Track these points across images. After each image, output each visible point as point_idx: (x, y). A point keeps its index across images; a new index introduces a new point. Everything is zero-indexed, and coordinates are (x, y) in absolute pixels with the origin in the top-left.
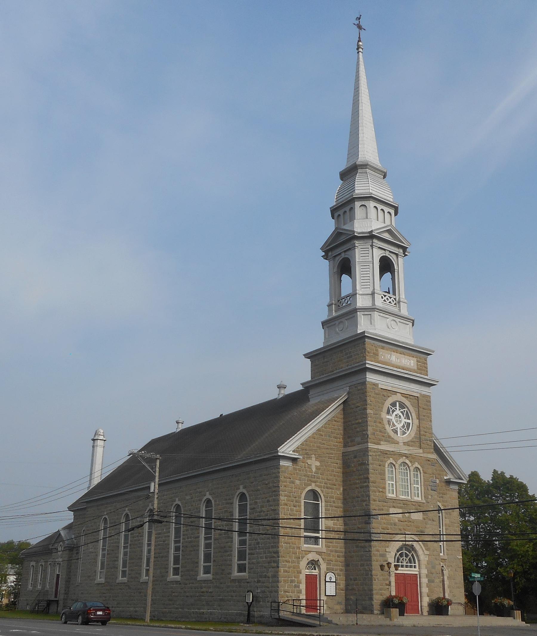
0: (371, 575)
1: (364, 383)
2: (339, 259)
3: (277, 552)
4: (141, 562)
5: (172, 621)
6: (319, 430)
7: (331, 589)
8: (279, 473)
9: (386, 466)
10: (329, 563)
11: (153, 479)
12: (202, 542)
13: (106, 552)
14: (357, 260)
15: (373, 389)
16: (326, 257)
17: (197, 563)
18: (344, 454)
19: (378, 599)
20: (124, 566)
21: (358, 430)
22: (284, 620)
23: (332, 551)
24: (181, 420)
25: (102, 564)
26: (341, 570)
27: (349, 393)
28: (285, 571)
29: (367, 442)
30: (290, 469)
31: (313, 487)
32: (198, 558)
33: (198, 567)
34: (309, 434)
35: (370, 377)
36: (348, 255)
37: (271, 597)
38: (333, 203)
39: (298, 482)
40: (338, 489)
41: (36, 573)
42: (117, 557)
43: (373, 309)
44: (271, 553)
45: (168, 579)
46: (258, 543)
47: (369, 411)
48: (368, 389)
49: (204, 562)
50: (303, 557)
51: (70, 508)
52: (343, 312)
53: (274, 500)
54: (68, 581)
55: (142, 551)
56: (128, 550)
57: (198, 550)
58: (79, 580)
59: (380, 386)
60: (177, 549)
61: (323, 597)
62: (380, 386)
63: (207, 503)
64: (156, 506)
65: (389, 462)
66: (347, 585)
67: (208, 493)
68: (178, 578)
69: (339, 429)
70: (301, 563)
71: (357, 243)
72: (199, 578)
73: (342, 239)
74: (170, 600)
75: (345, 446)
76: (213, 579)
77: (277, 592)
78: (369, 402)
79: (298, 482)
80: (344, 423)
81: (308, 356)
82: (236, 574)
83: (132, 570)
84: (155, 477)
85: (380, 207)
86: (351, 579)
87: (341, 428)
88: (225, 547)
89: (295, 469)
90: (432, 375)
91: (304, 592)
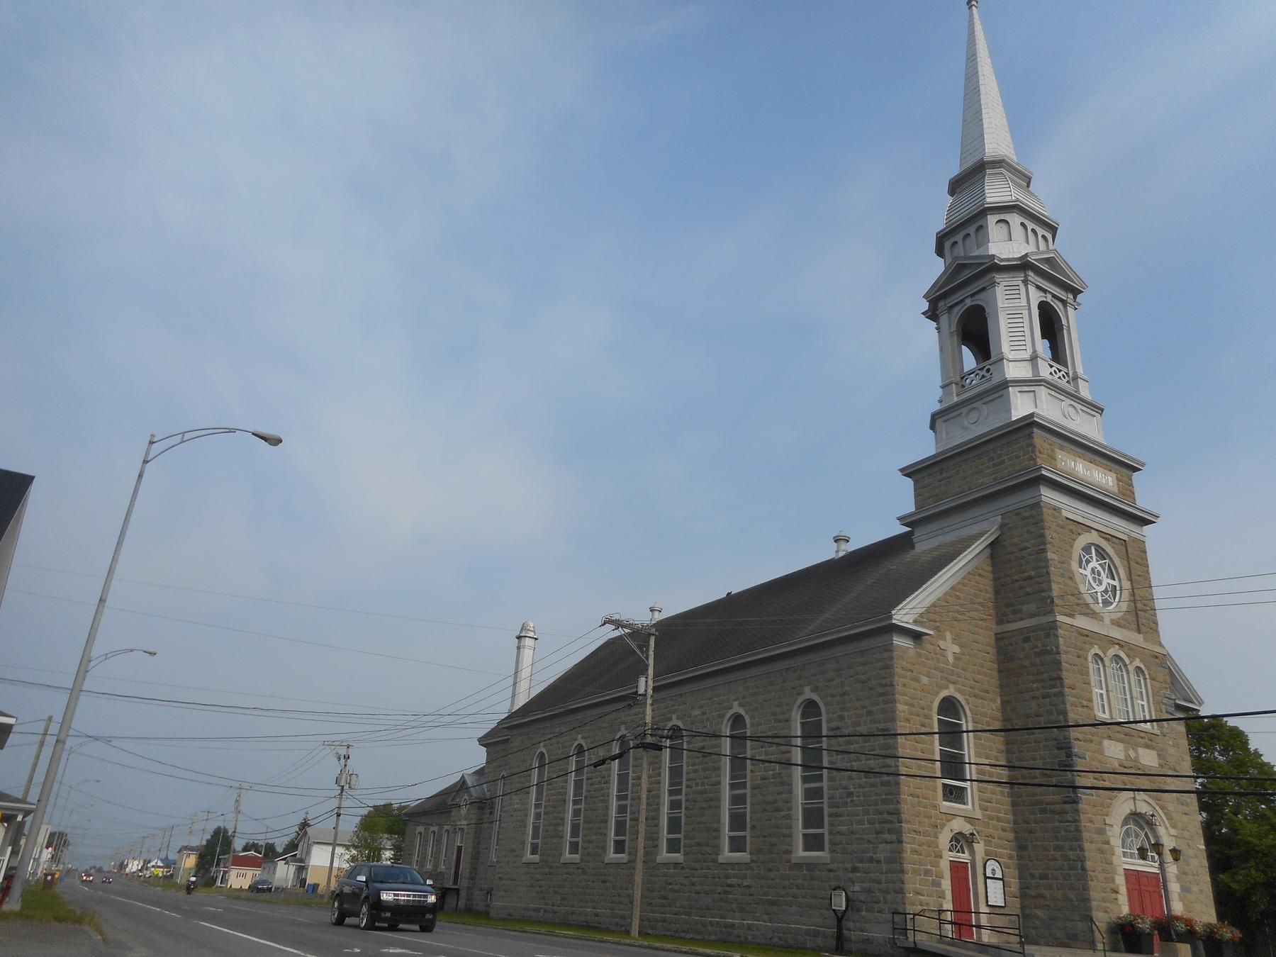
0: (1083, 869)
1: (1037, 505)
2: (958, 312)
3: (897, 813)
4: (606, 828)
5: (665, 937)
6: (953, 588)
7: (996, 894)
8: (891, 658)
9: (1090, 658)
10: (989, 839)
11: (644, 671)
12: (726, 793)
13: (542, 810)
14: (1000, 305)
15: (1054, 517)
16: (932, 315)
17: (717, 830)
18: (999, 637)
19: (1102, 919)
20: (575, 832)
21: (1029, 589)
22: (924, 951)
23: (991, 818)
24: (657, 607)
25: (536, 829)
26: (1010, 857)
27: (1001, 526)
28: (915, 852)
29: (1052, 612)
30: (911, 653)
31: (950, 691)
32: (718, 821)
33: (718, 837)
34: (939, 593)
35: (1049, 496)
36: (980, 300)
37: (886, 902)
38: (940, 224)
39: (925, 680)
40: (995, 701)
41: (424, 845)
42: (563, 819)
43: (1037, 382)
44: (881, 813)
45: (659, 859)
46: (850, 795)
47: (1050, 555)
48: (1046, 517)
49: (731, 830)
50: (943, 826)
51: (483, 741)
52: (975, 389)
53: (884, 711)
54: (476, 856)
55: (607, 808)
56: (582, 806)
57: (718, 807)
58: (364, 909)
59: (1065, 513)
60: (675, 805)
61: (983, 908)
62: (1065, 513)
63: (734, 722)
64: (648, 719)
65: (1093, 651)
66: (1024, 888)
67: (736, 703)
68: (678, 857)
69: (987, 591)
70: (941, 836)
71: (999, 277)
72: (721, 859)
73: (966, 274)
74: (664, 898)
75: (1000, 622)
76: (752, 861)
77: (901, 891)
78: (1048, 538)
79: (925, 680)
80: (995, 580)
81: (909, 472)
82: (800, 853)
83: (589, 842)
84: (646, 667)
85: (1030, 225)
86: (1033, 876)
87: (990, 589)
88: (775, 801)
89: (919, 655)
90: (1144, 501)
91: (949, 895)
